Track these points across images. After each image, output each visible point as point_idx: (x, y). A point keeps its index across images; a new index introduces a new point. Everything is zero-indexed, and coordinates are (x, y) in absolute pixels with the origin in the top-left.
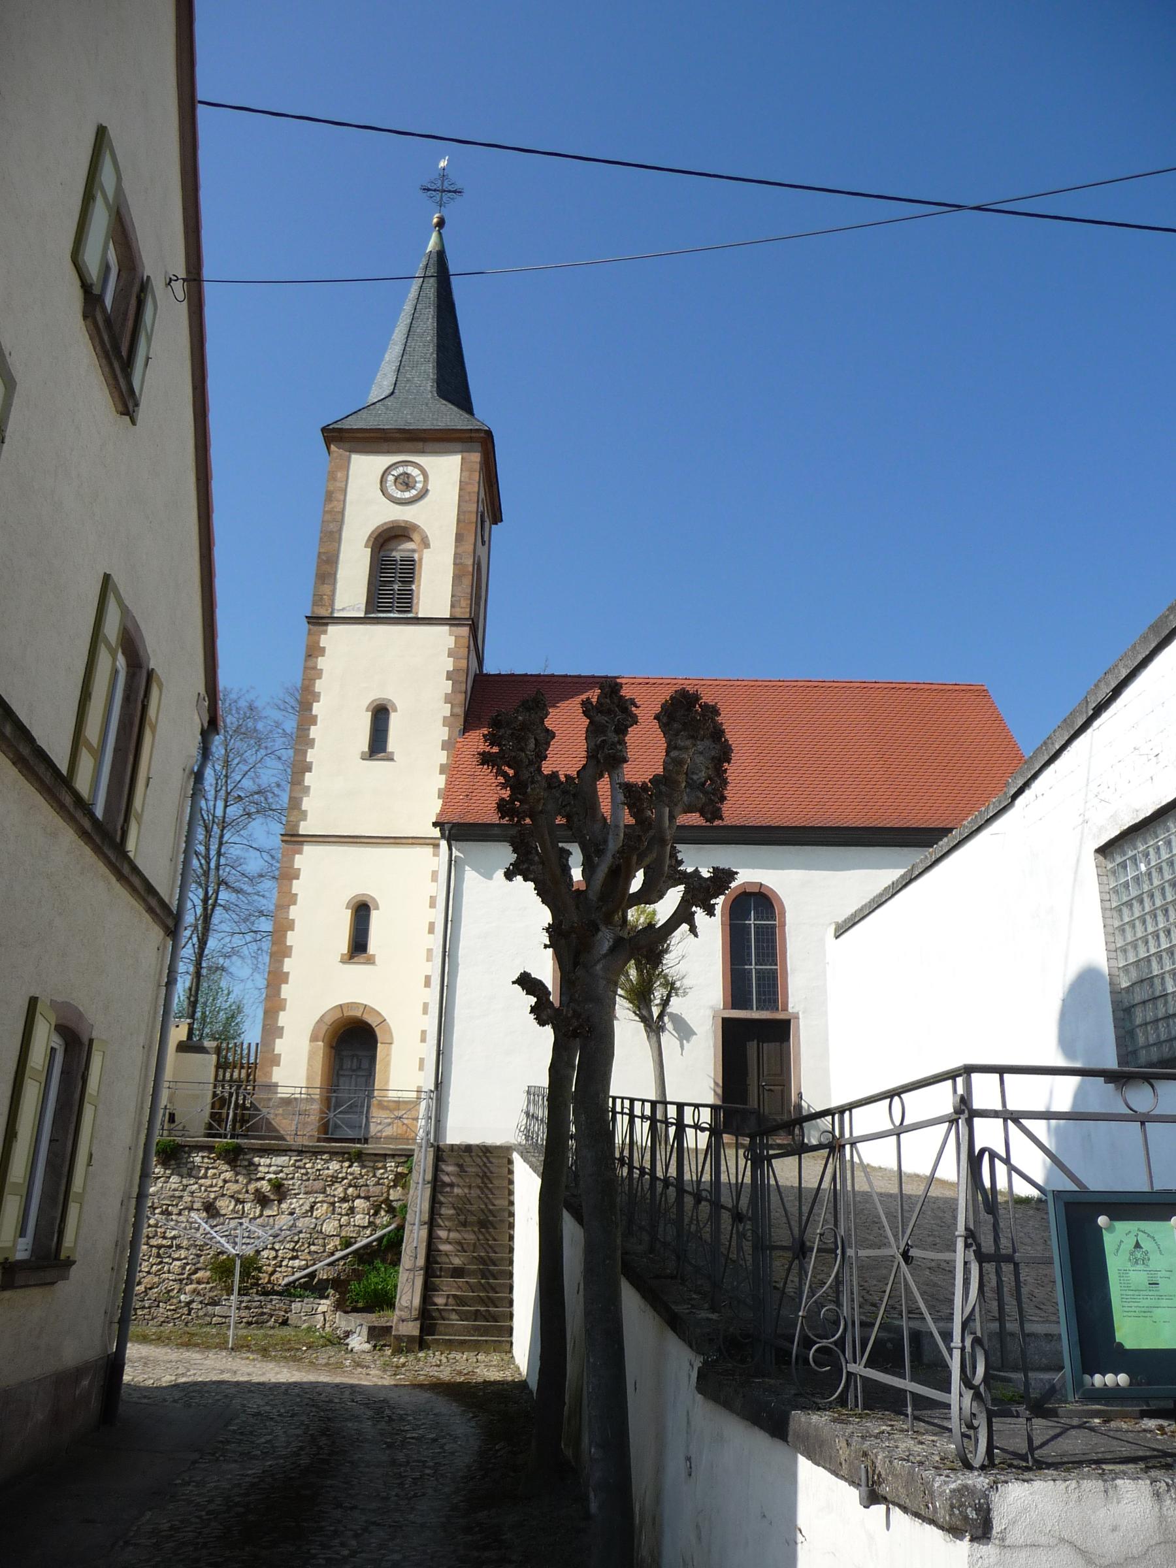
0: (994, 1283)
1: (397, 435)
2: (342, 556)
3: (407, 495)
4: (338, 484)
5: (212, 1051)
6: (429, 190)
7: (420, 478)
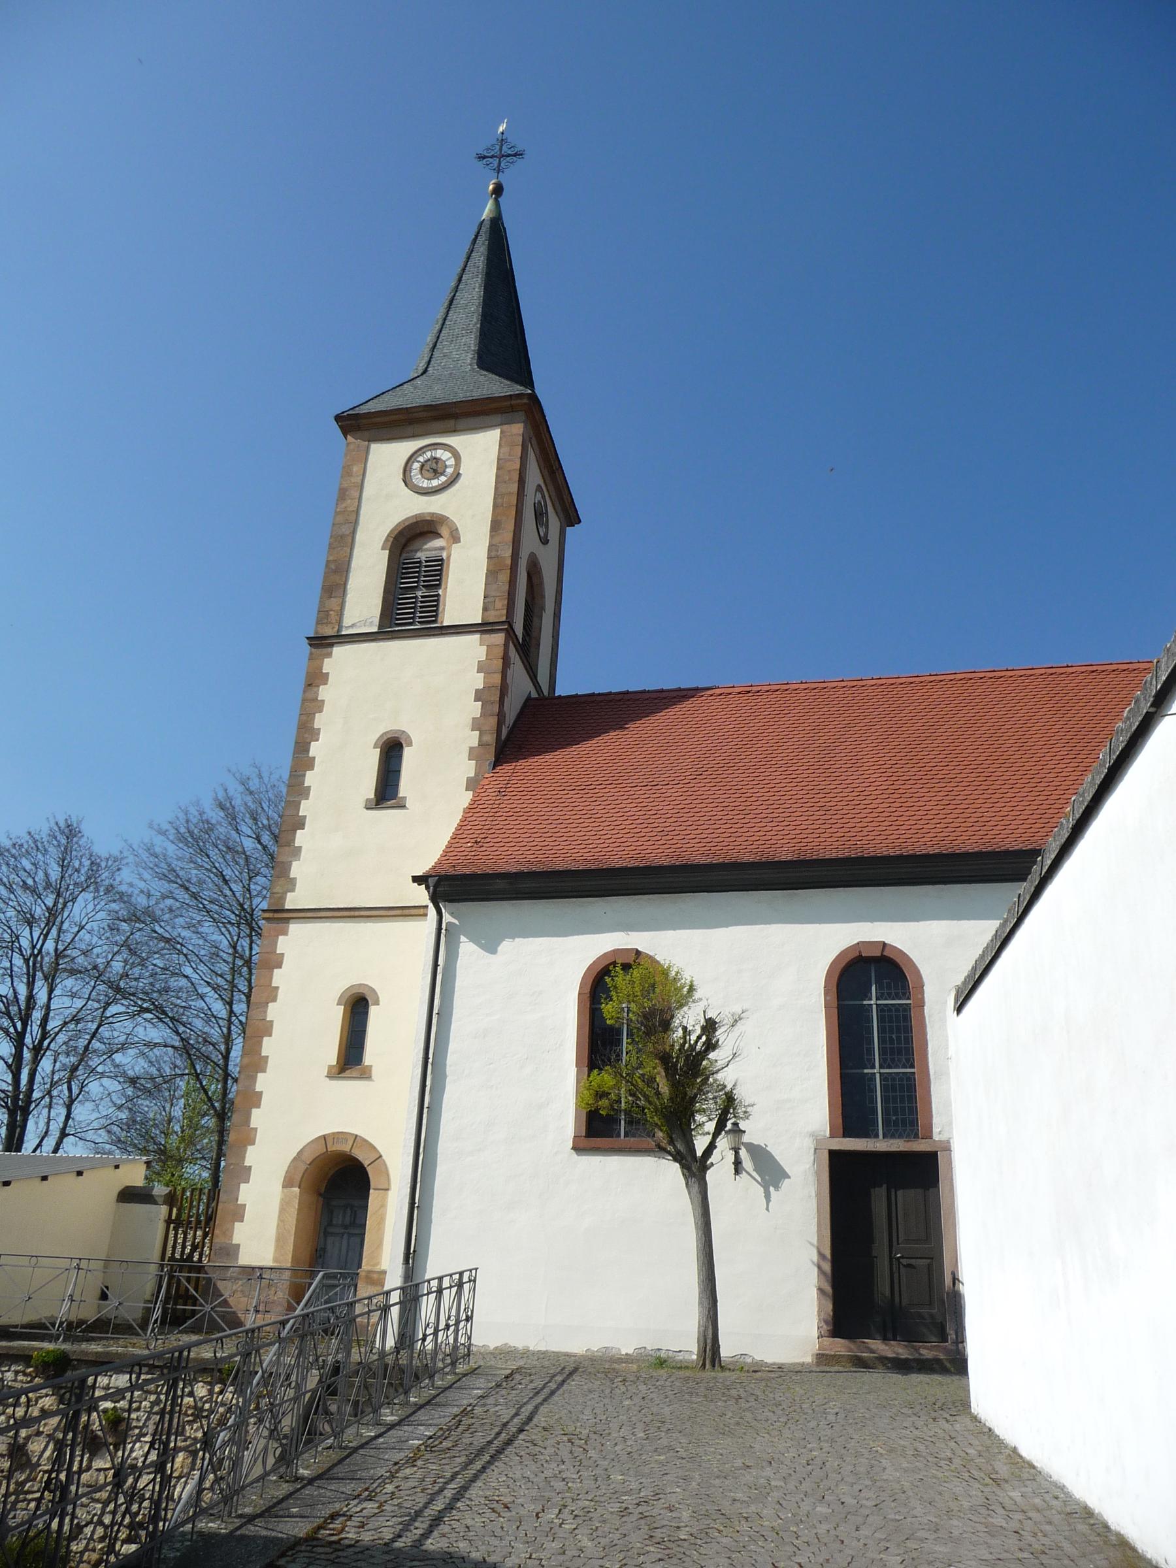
1: (425, 414)
2: (354, 563)
3: (435, 483)
4: (353, 480)
5: (160, 1200)
6: (484, 157)
7: (452, 462)
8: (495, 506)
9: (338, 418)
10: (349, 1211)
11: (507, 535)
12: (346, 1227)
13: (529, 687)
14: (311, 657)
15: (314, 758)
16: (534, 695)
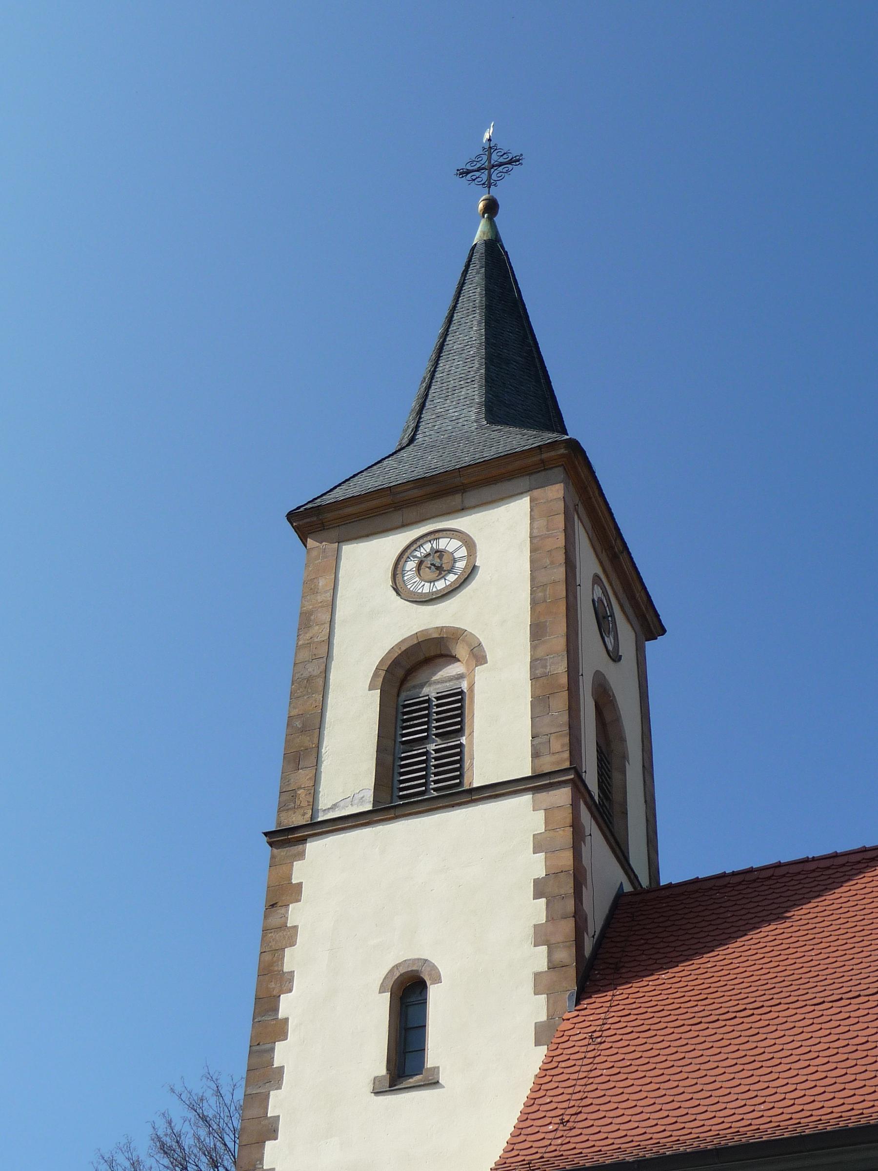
1: (416, 493)
2: (330, 715)
3: (440, 585)
4: (320, 598)
6: (468, 172)
7: (463, 552)
8: (534, 603)
9: (291, 516)
11: (558, 641)
13: (618, 876)
14: (273, 863)
15: (286, 1020)
16: (628, 888)
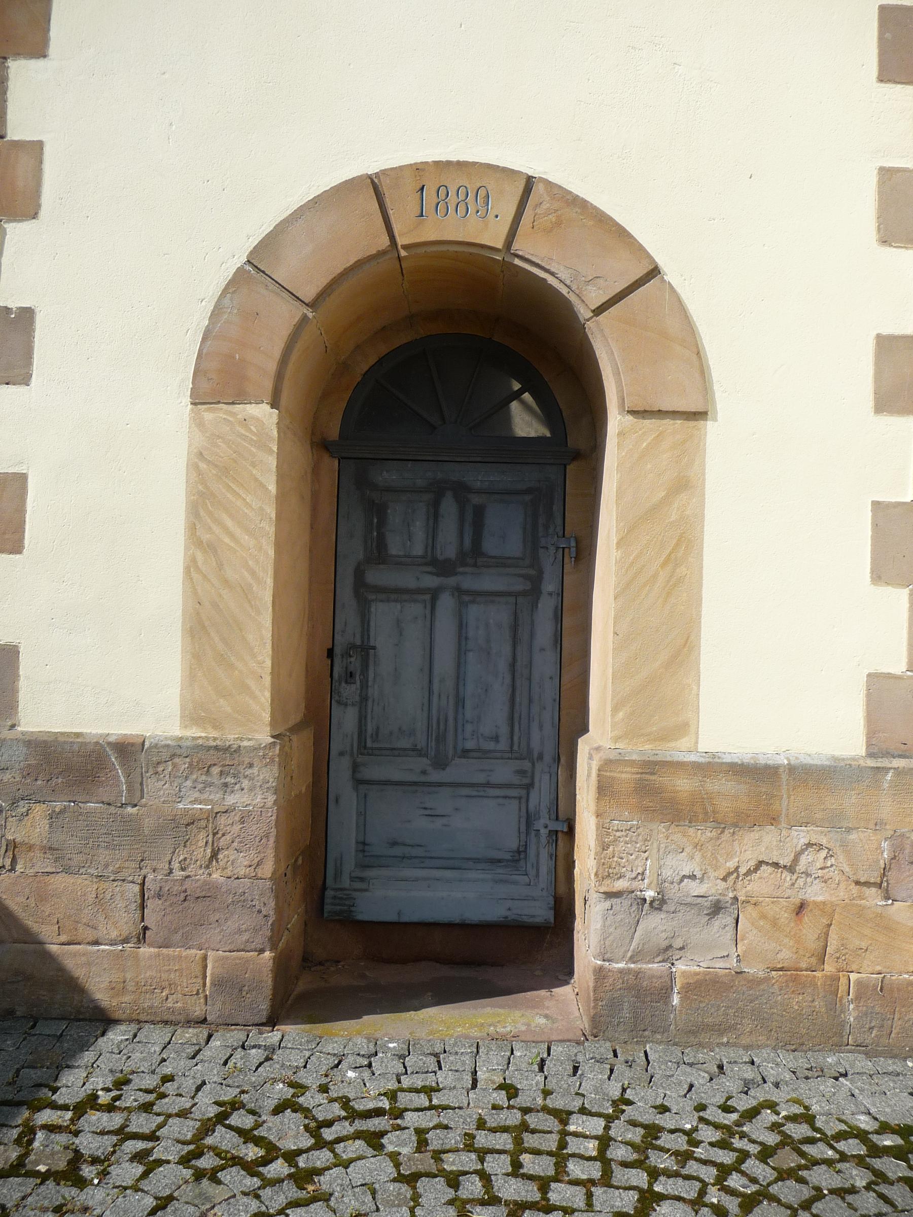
0: (555, 508)
10: (449, 507)
12: (444, 568)
